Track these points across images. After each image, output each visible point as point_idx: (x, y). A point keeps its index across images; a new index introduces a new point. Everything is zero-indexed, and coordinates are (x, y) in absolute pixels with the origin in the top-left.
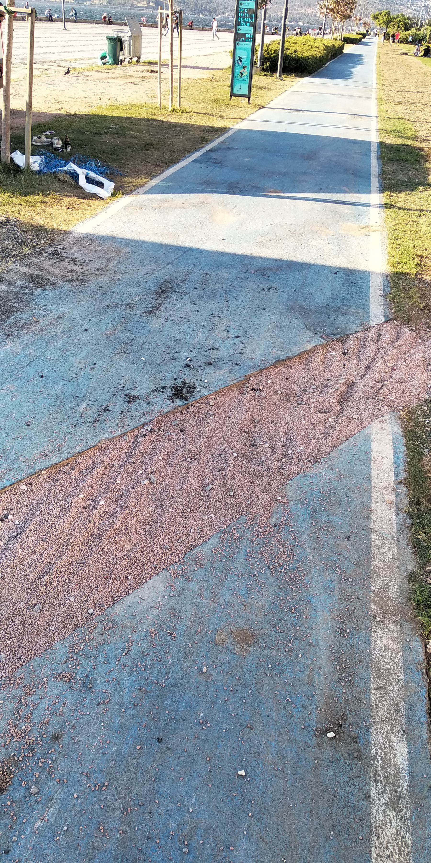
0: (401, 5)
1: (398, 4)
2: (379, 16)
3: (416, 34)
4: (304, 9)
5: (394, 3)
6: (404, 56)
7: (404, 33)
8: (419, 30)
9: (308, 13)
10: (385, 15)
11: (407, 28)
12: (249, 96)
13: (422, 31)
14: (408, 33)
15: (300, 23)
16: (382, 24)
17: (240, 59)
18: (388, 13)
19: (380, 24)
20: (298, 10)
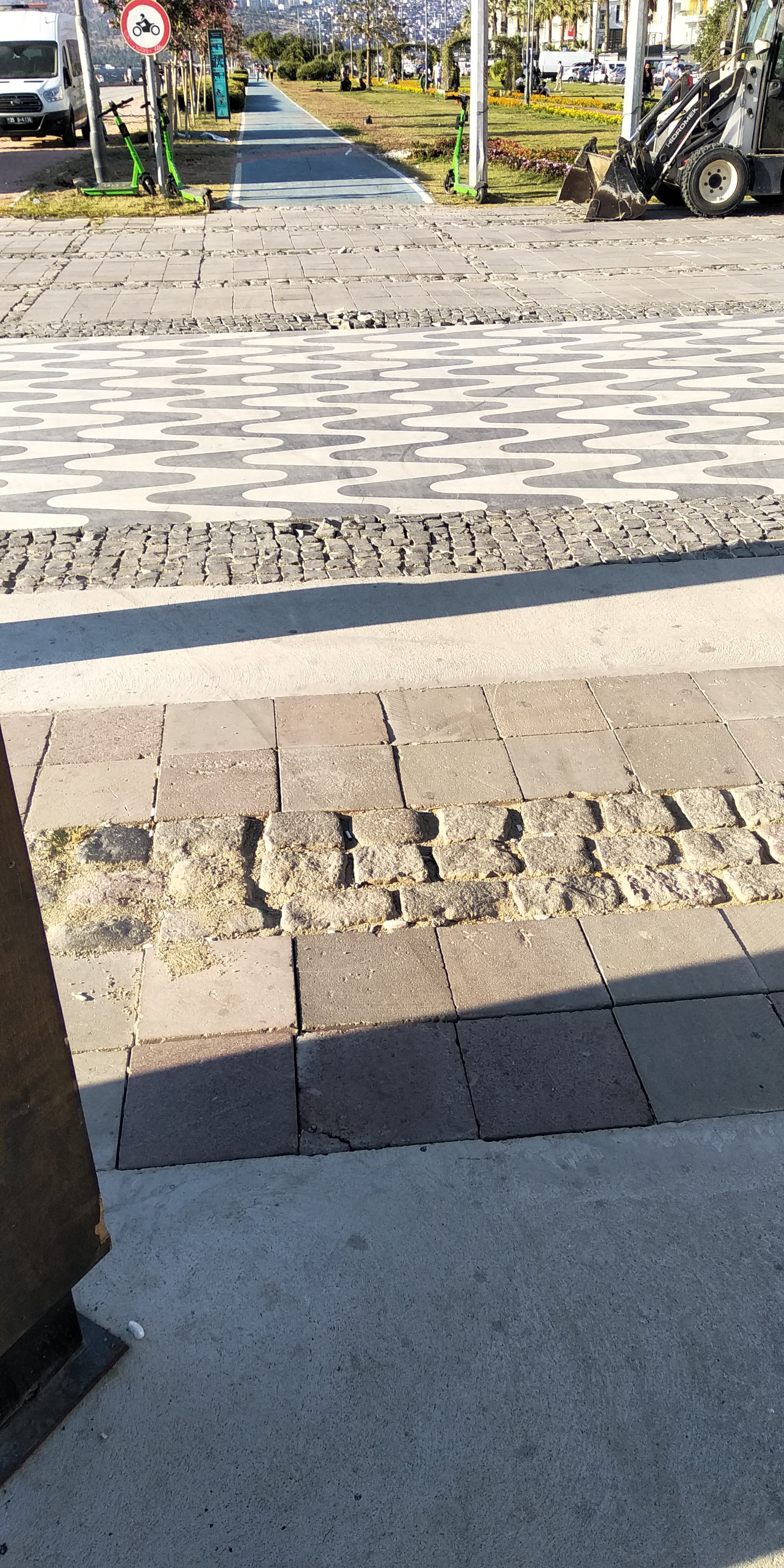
0: (280, 17)
1: (273, 17)
2: (255, 43)
3: (323, 65)
4: (109, 40)
5: (267, 15)
6: (319, 93)
7: (306, 65)
8: (325, 58)
9: (117, 46)
10: (264, 39)
11: (308, 58)
12: (229, 118)
13: (329, 60)
14: (310, 64)
15: (108, 67)
16: (263, 55)
17: (219, 91)
18: (269, 36)
19: (259, 55)
20: (98, 43)
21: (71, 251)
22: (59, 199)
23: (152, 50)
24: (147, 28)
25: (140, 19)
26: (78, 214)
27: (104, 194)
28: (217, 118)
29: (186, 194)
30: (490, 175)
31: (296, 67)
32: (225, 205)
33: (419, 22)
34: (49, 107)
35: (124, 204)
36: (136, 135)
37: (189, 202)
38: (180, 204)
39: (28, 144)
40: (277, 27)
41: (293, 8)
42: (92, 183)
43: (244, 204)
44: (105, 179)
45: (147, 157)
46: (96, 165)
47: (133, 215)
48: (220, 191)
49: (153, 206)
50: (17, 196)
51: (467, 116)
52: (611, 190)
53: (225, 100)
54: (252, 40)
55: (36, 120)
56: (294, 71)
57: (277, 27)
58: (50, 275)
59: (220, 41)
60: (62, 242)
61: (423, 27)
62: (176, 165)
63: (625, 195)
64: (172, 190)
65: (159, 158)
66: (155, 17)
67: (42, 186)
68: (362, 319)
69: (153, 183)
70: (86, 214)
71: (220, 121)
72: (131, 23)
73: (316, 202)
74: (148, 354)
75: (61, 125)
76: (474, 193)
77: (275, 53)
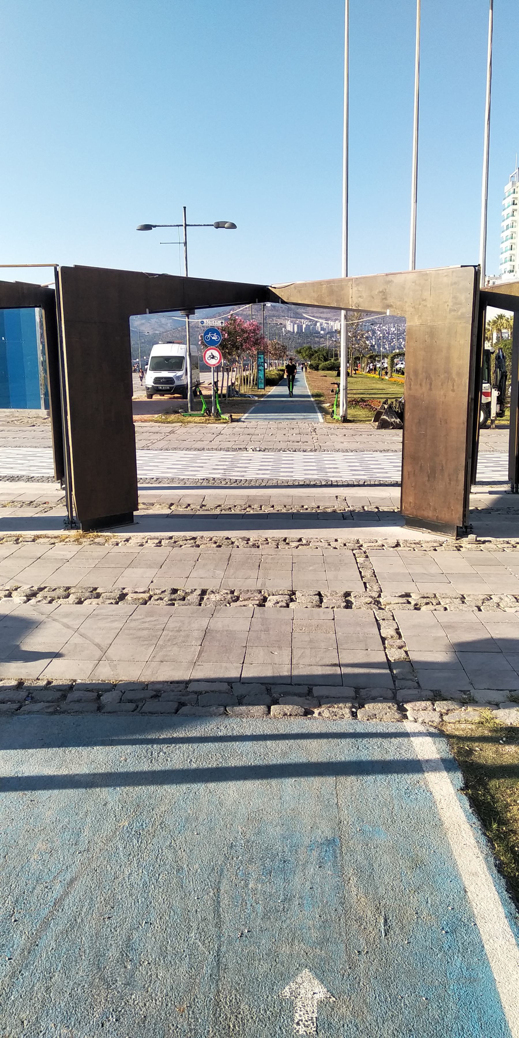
0: (321, 338)
1: (317, 337)
10: (307, 350)
11: (326, 360)
14: (326, 363)
21: (172, 432)
22: (172, 417)
23: (214, 365)
24: (213, 357)
25: (210, 354)
26: (178, 422)
27: (190, 415)
28: (258, 389)
29: (222, 416)
30: (349, 411)
31: (319, 364)
32: (238, 420)
33: (401, 340)
34: (177, 383)
35: (197, 419)
36: (206, 395)
37: (223, 419)
38: (220, 420)
39: (166, 398)
40: (319, 342)
41: (328, 333)
42: (186, 411)
43: (245, 420)
44: (192, 410)
45: (209, 403)
46: (189, 405)
47: (200, 423)
48: (235, 416)
49: (209, 420)
50: (156, 416)
51: (339, 390)
52: (387, 418)
53: (263, 381)
54: (301, 350)
55: (171, 388)
56: (318, 366)
57: (319, 342)
58: (162, 438)
59: (263, 356)
60: (169, 429)
61: (403, 343)
62: (220, 406)
63: (392, 420)
64: (218, 415)
65: (213, 404)
66: (216, 354)
67: (167, 413)
68: (258, 449)
69: (210, 412)
70: (182, 422)
71: (259, 390)
72: (207, 356)
73: (275, 421)
74: (185, 454)
75: (182, 390)
76: (340, 418)
77: (310, 356)
